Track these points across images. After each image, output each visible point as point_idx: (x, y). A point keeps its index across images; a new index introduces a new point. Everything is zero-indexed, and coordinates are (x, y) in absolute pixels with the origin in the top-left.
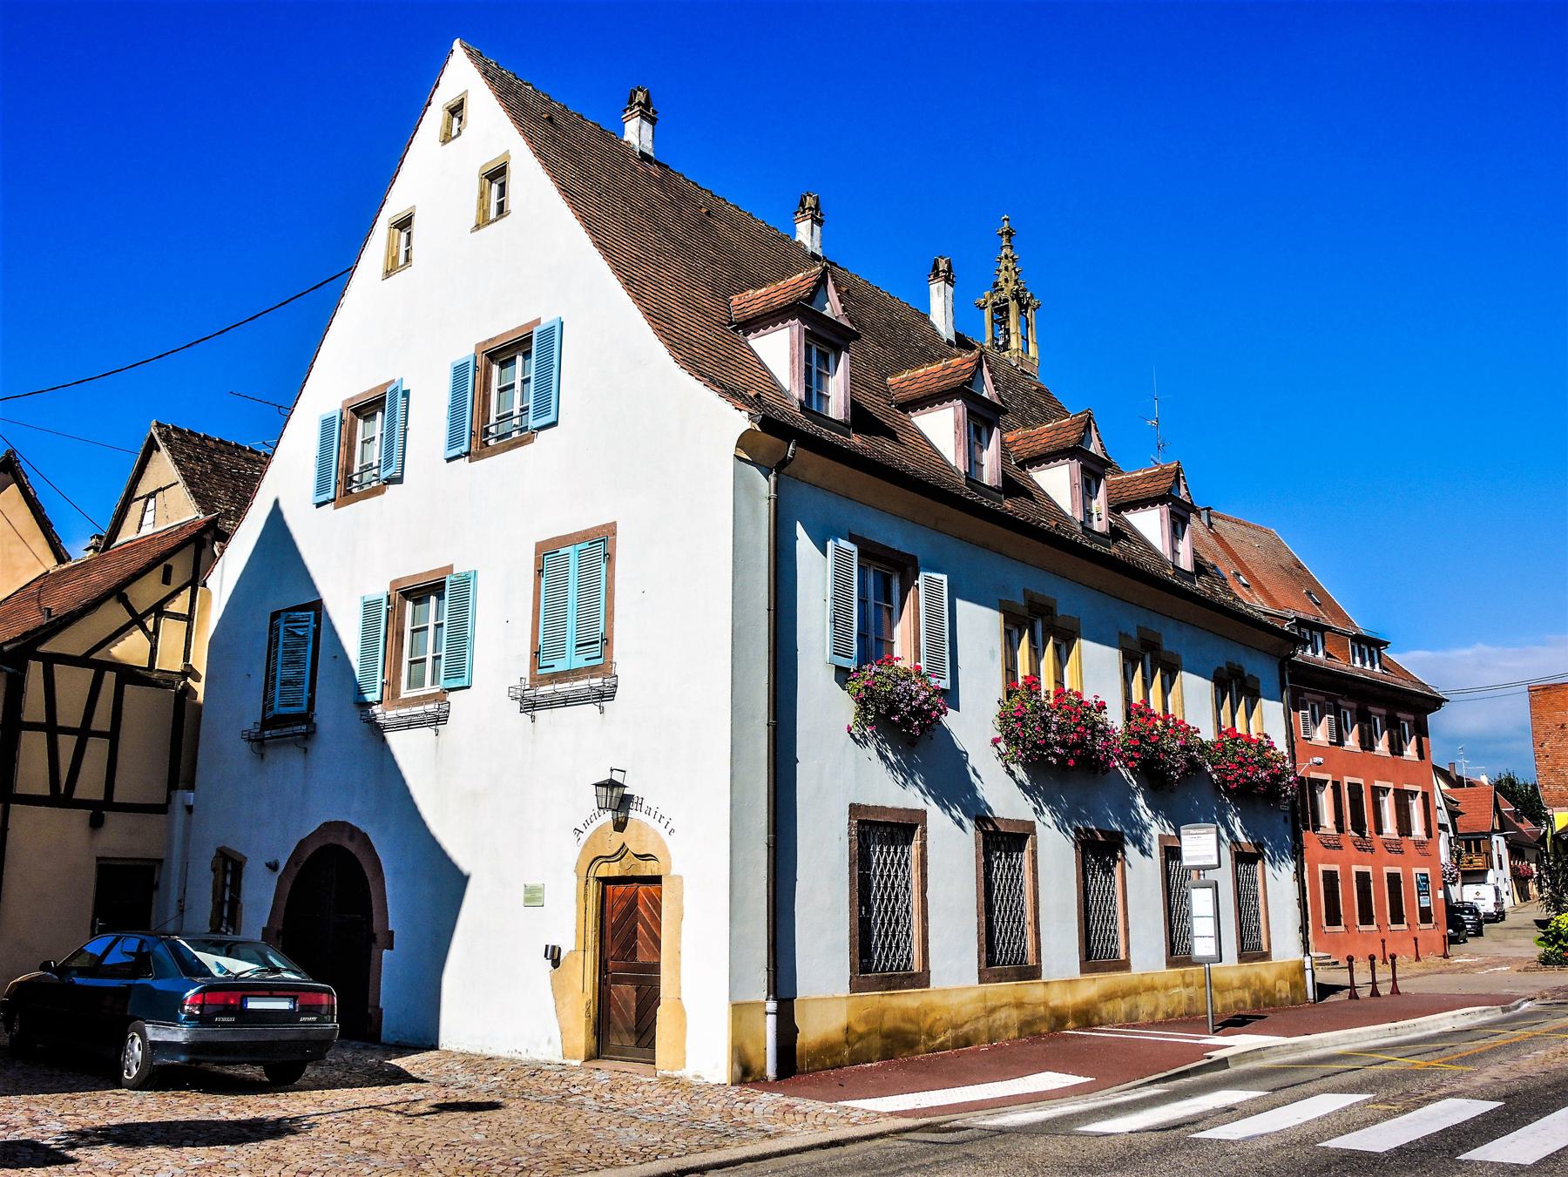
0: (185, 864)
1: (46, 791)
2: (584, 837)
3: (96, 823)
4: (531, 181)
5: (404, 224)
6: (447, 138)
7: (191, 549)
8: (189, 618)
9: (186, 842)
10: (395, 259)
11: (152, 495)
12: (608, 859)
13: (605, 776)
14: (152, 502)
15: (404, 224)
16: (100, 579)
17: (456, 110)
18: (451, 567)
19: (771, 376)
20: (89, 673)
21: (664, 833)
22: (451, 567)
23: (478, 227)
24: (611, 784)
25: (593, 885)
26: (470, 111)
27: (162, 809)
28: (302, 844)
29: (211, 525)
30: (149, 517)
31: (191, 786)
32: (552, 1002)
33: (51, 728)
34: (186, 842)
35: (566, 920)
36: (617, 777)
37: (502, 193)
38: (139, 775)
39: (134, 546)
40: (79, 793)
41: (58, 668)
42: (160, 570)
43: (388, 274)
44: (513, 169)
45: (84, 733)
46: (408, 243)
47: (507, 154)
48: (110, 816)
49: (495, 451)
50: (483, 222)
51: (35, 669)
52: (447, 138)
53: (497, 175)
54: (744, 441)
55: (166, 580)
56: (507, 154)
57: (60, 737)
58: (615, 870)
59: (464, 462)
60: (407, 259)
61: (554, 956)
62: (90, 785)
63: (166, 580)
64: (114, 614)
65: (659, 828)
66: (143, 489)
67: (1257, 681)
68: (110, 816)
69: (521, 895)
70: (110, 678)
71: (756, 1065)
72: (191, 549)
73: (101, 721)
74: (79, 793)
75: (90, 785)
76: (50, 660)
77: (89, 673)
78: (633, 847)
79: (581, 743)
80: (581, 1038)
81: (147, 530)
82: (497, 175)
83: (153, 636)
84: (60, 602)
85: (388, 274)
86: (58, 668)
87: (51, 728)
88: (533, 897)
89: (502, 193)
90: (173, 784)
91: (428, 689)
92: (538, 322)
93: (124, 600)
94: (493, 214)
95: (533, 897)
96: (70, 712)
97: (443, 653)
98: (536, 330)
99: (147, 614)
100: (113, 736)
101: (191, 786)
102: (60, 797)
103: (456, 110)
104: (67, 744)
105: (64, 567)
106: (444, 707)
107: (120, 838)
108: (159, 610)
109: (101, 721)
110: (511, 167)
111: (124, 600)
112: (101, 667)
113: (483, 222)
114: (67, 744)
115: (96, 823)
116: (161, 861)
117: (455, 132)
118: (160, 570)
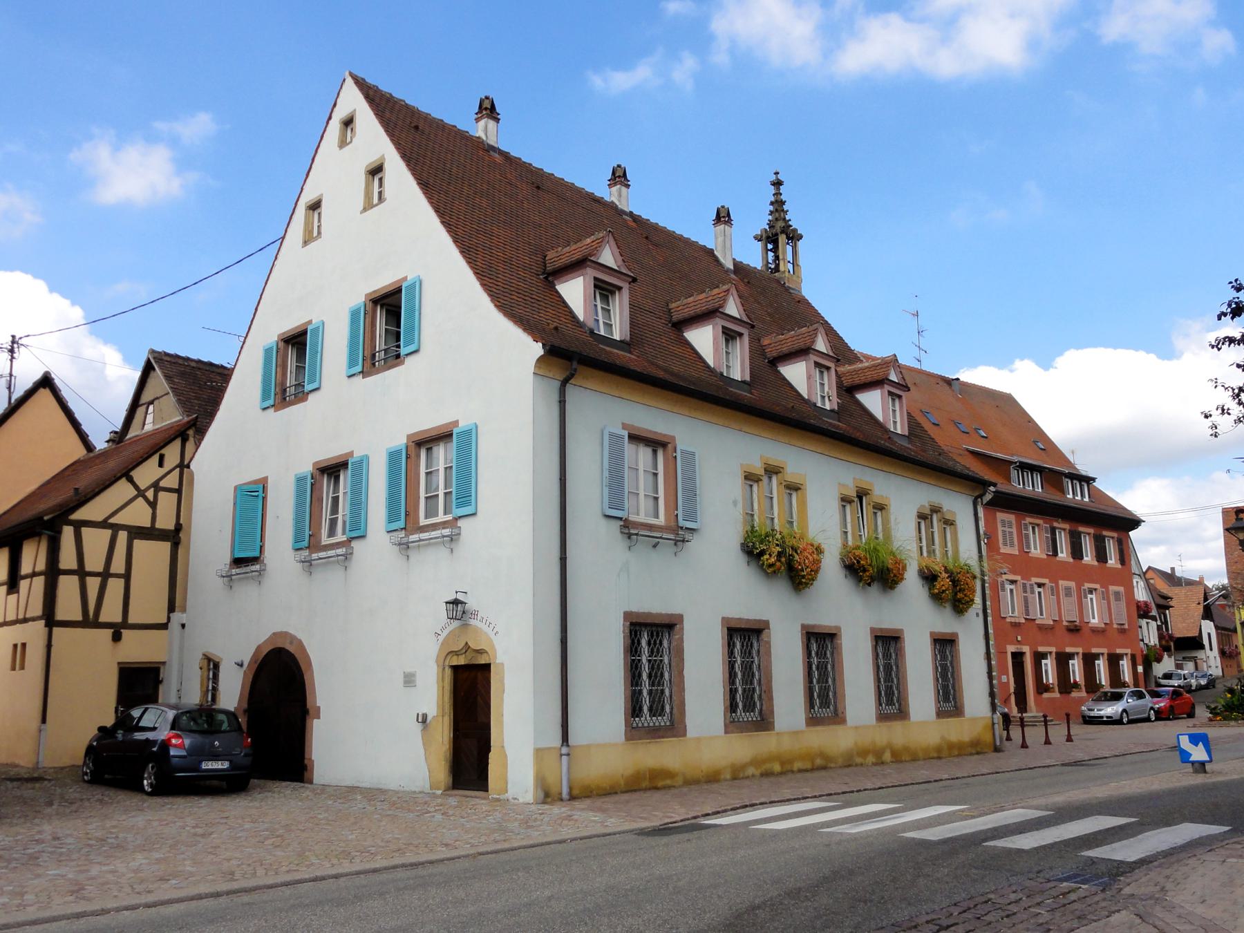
0: (181, 665)
1: (78, 616)
2: (441, 638)
3: (117, 637)
4: (399, 175)
5: (315, 206)
6: (343, 143)
7: (178, 443)
8: (178, 491)
9: (181, 649)
10: (311, 232)
11: (151, 402)
12: (457, 653)
13: (451, 597)
14: (151, 408)
15: (315, 206)
16: (113, 464)
17: (348, 122)
18: (457, 422)
19: (571, 312)
20: (108, 532)
21: (492, 635)
22: (457, 422)
23: (365, 210)
24: (456, 602)
25: (448, 672)
26: (358, 122)
27: (164, 626)
28: (259, 647)
29: (193, 424)
30: (150, 418)
31: (184, 610)
32: (422, 751)
33: (81, 572)
34: (181, 649)
35: (431, 696)
36: (460, 597)
37: (381, 185)
38: (148, 601)
39: (138, 440)
40: (103, 618)
41: (84, 530)
42: (156, 458)
43: (306, 243)
44: (387, 167)
45: (105, 575)
46: (319, 221)
47: (383, 157)
48: (125, 632)
49: (291, 403)
50: (368, 206)
51: (68, 532)
52: (343, 143)
53: (376, 171)
54: (540, 360)
55: (161, 465)
56: (383, 157)
57: (123, 572)
58: (461, 661)
59: (272, 410)
60: (319, 233)
61: (424, 720)
62: (111, 612)
63: (161, 465)
64: (122, 490)
65: (489, 631)
66: (145, 398)
67: (954, 514)
68: (125, 632)
69: (401, 679)
70: (123, 536)
71: (554, 790)
72: (178, 443)
73: (118, 566)
74: (103, 618)
75: (111, 612)
76: (79, 525)
77: (108, 532)
78: (472, 645)
79: (434, 576)
80: (442, 774)
81: (149, 427)
82: (376, 171)
83: (153, 505)
84: (84, 481)
85: (306, 243)
86: (84, 530)
87: (81, 572)
88: (409, 680)
89: (381, 185)
90: (171, 608)
91: (441, 517)
92: (405, 279)
93: (131, 480)
94: (376, 200)
95: (409, 680)
96: (94, 562)
97: (453, 489)
98: (310, 328)
99: (148, 489)
100: (127, 576)
101: (184, 610)
102: (90, 621)
103: (348, 122)
104: (93, 584)
105: (91, 455)
106: (456, 531)
107: (137, 648)
108: (156, 486)
109: (118, 566)
110: (386, 166)
111: (131, 480)
112: (116, 528)
113: (368, 206)
114: (93, 584)
115: (117, 637)
116: (164, 663)
117: (349, 140)
118: (156, 458)
